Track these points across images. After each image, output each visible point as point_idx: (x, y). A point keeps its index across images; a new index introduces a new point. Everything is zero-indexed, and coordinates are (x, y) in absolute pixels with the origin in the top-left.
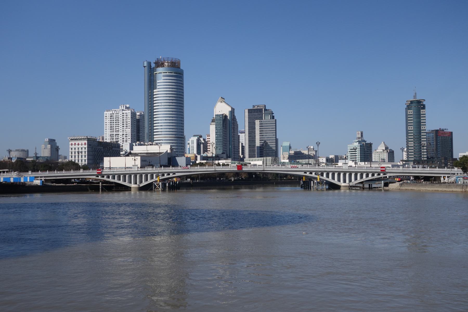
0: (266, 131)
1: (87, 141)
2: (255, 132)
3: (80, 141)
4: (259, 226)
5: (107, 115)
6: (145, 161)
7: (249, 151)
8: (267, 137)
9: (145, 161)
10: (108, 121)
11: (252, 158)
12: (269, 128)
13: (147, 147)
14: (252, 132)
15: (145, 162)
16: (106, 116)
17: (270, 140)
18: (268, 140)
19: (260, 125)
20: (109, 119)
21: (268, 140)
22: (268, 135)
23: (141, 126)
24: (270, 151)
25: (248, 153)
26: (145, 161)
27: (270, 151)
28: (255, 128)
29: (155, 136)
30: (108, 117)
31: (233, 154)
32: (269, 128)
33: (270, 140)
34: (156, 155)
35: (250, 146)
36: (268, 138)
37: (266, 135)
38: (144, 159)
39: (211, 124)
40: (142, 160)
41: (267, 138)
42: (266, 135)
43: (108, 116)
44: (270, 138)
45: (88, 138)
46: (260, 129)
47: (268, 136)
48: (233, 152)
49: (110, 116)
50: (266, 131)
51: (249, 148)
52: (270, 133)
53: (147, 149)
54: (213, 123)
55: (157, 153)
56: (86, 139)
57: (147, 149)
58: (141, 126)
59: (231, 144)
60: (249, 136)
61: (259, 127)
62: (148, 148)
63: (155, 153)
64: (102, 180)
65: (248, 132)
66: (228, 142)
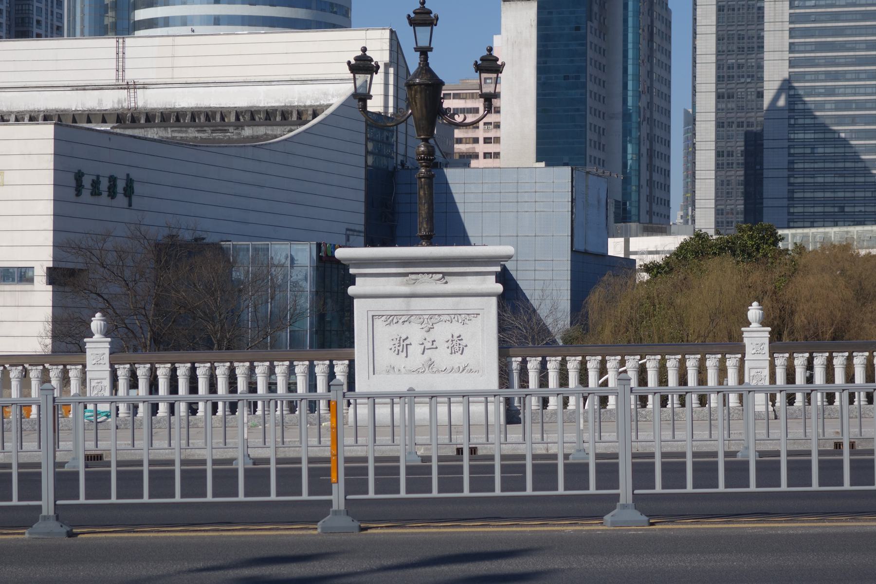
0: (832, 62)
2: (760, 67)
3: (206, 352)
4: (67, 289)
6: (121, 185)
7: (717, 189)
8: (837, 102)
9: (112, 193)
11: (836, 224)
12: (853, 46)
13: (120, 56)
14: (740, 66)
15: (121, 199)
17: (853, 120)
18: (841, 120)
19: (791, 22)
21: (841, 120)
22: (845, 87)
23: (38, 22)
24: (855, 187)
25: (712, 204)
26: (121, 185)
27: (855, 187)
28: (761, 47)
31: (644, 205)
32: (853, 46)
33: (853, 120)
34: (232, 133)
35: (725, 159)
36: (847, 105)
37: (831, 92)
38: (105, 171)
40: (79, 176)
41: (839, 106)
42: (831, 92)
44: (857, 109)
46: (792, 48)
47: (845, 95)
48: (645, 191)
50: (832, 62)
51: (719, 167)
52: (857, 76)
53: (120, 69)
55: (239, 113)
57: (120, 69)
58: (38, 22)
59: (634, 133)
60: (719, 97)
61: (787, 41)
62: (128, 64)
63: (223, 113)
64: (663, 28)
65: (714, 66)
66: (618, 124)
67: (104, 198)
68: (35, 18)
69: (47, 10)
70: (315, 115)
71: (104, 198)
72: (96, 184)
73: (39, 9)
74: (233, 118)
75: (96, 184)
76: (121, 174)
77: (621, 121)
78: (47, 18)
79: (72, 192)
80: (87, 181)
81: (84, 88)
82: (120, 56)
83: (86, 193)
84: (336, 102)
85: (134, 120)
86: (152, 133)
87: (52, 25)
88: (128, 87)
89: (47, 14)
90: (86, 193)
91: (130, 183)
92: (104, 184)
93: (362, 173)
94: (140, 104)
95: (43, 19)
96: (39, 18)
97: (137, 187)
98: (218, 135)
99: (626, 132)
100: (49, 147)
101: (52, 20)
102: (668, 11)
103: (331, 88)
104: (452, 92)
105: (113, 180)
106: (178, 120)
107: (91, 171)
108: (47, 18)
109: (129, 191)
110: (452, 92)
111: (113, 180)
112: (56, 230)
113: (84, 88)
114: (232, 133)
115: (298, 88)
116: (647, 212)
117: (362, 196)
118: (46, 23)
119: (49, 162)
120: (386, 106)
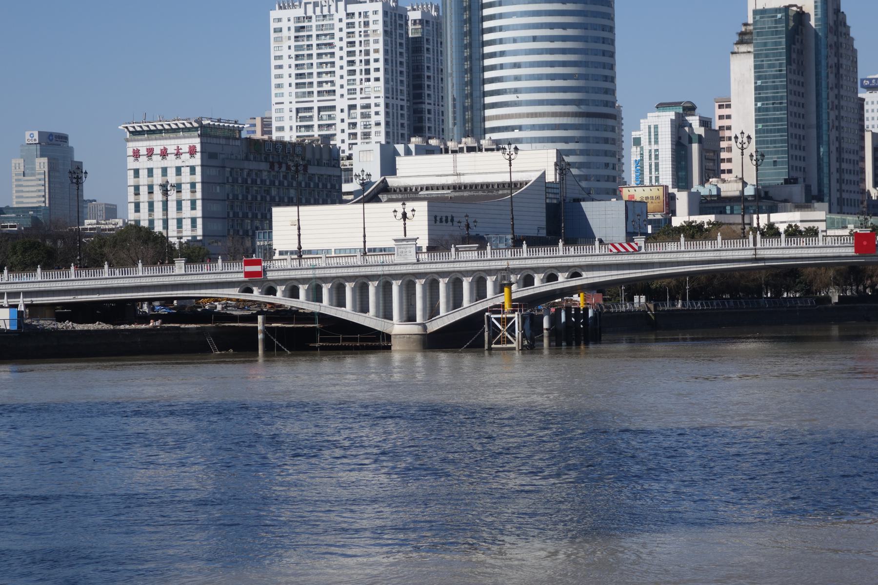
1: (198, 140)
5: (284, 25)
6: (449, 219)
10: (285, 52)
13: (455, 161)
15: (450, 223)
16: (276, 31)
20: (293, 43)
26: (449, 219)
29: (488, 113)
30: (285, 33)
31: (835, 186)
34: (495, 193)
38: (444, 214)
39: (733, 53)
40: (436, 217)
43: (285, 30)
45: (202, 126)
48: (835, 176)
49: (293, 29)
53: (455, 167)
54: (743, 48)
55: (499, 184)
56: (196, 129)
57: (455, 167)
58: (428, 68)
59: (825, 138)
63: (493, 185)
66: (814, 132)
67: (444, 223)
68: (426, 65)
69: (434, 58)
70: (526, 184)
71: (444, 223)
72: (441, 219)
73: (429, 59)
74: (496, 187)
75: (441, 219)
76: (449, 215)
77: (815, 130)
78: (434, 64)
79: (433, 222)
80: (438, 219)
81: (441, 176)
82: (455, 161)
83: (438, 222)
84: (534, 179)
85: (460, 188)
86: (466, 194)
87: (438, 68)
88: (457, 175)
89: (434, 61)
90: (438, 222)
91: (452, 217)
92: (444, 219)
93: (544, 206)
94: (462, 181)
95: (431, 65)
96: (429, 65)
97: (455, 219)
98: (490, 194)
99: (819, 137)
100: (426, 209)
101: (438, 65)
102: (854, 51)
103: (532, 174)
104: (725, 103)
105: (447, 217)
106: (476, 188)
107: (439, 215)
108: (434, 64)
109: (452, 220)
110: (725, 103)
111: (447, 217)
112: (429, 235)
113: (441, 176)
114: (495, 193)
115: (520, 174)
116: (838, 190)
117: (544, 215)
118: (434, 68)
119: (426, 213)
120: (556, 179)
